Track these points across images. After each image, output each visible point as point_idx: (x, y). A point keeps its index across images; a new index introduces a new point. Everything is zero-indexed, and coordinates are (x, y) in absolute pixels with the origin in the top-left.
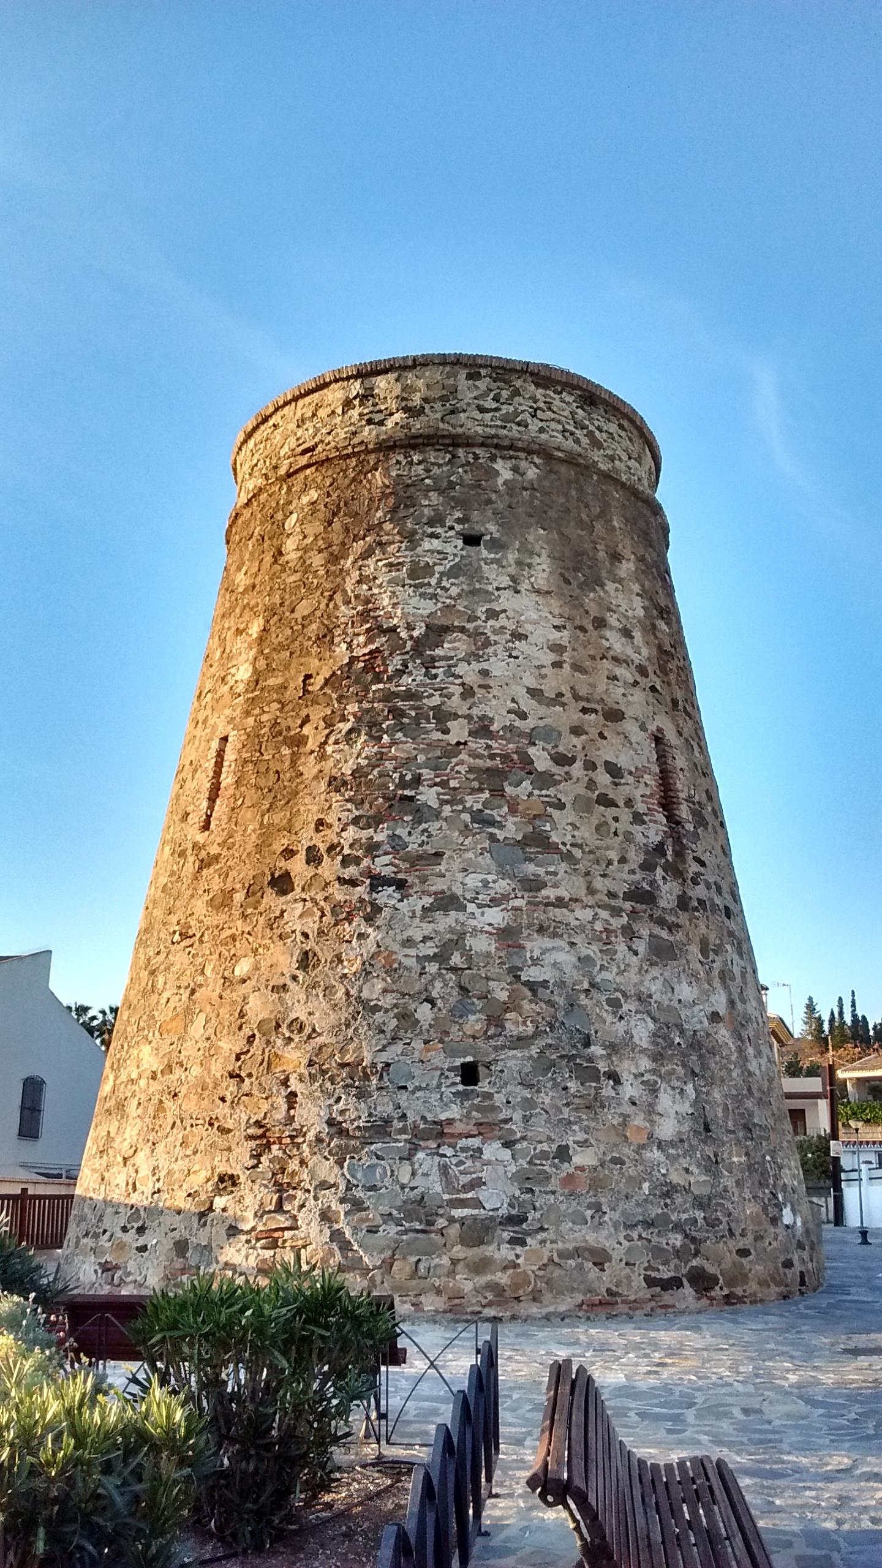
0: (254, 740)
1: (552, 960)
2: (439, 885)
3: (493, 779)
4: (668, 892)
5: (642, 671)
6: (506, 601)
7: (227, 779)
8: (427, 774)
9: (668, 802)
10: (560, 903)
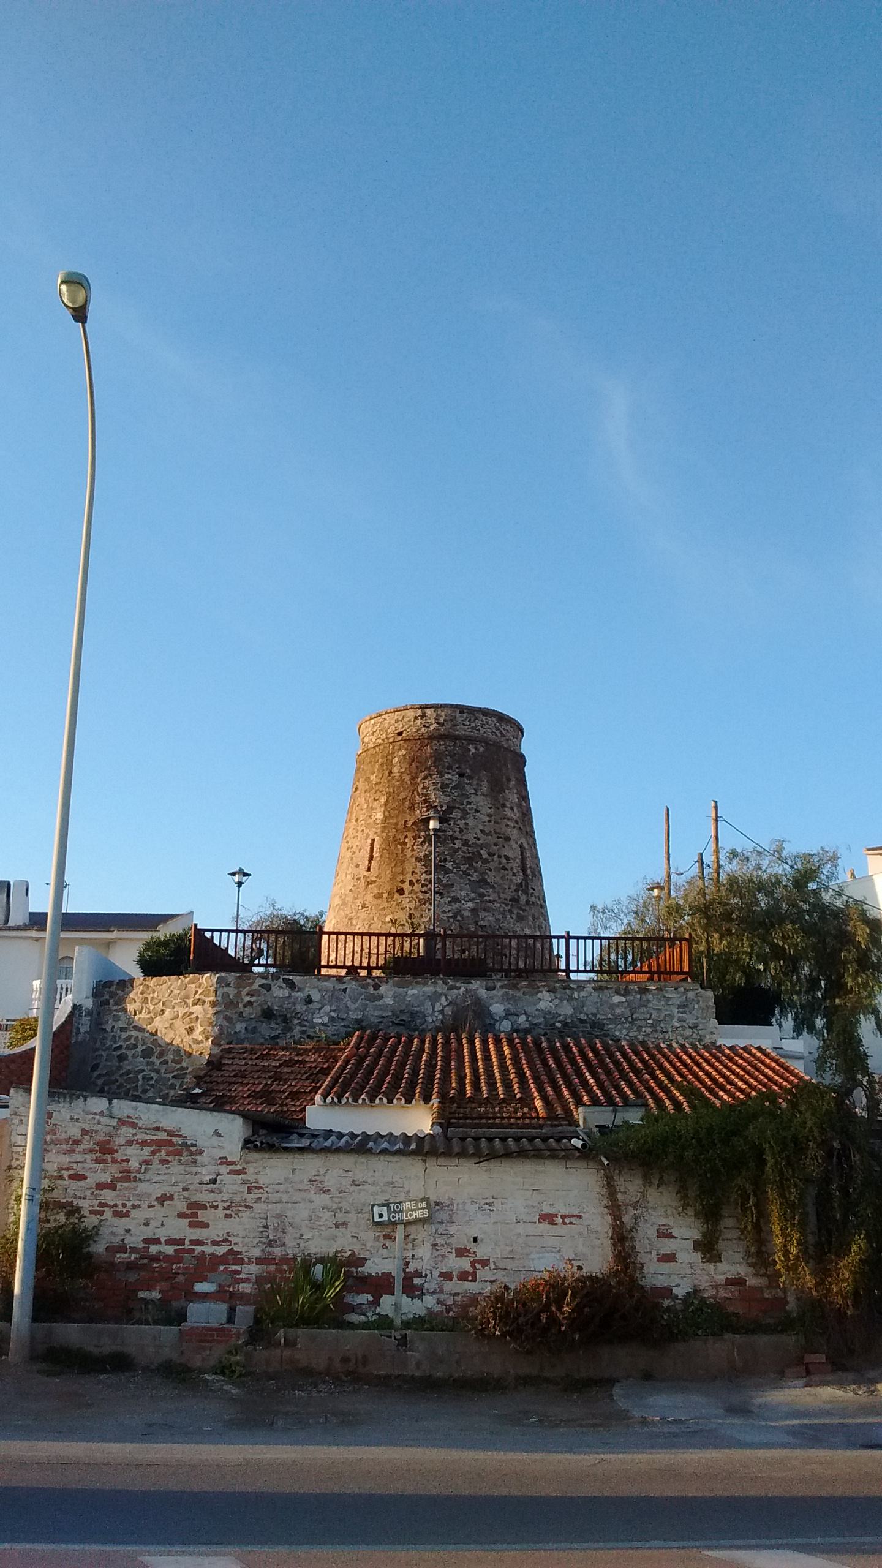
0: (386, 841)
1: (487, 919)
2: (453, 895)
3: (469, 860)
4: (523, 899)
5: (517, 822)
6: (473, 798)
7: (376, 854)
8: (448, 858)
9: (524, 869)
10: (490, 901)
